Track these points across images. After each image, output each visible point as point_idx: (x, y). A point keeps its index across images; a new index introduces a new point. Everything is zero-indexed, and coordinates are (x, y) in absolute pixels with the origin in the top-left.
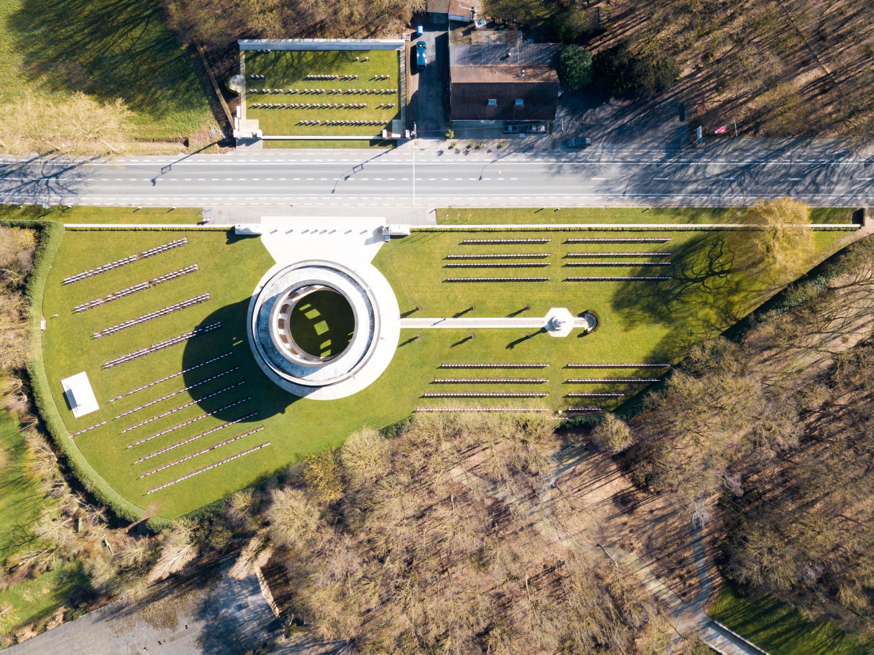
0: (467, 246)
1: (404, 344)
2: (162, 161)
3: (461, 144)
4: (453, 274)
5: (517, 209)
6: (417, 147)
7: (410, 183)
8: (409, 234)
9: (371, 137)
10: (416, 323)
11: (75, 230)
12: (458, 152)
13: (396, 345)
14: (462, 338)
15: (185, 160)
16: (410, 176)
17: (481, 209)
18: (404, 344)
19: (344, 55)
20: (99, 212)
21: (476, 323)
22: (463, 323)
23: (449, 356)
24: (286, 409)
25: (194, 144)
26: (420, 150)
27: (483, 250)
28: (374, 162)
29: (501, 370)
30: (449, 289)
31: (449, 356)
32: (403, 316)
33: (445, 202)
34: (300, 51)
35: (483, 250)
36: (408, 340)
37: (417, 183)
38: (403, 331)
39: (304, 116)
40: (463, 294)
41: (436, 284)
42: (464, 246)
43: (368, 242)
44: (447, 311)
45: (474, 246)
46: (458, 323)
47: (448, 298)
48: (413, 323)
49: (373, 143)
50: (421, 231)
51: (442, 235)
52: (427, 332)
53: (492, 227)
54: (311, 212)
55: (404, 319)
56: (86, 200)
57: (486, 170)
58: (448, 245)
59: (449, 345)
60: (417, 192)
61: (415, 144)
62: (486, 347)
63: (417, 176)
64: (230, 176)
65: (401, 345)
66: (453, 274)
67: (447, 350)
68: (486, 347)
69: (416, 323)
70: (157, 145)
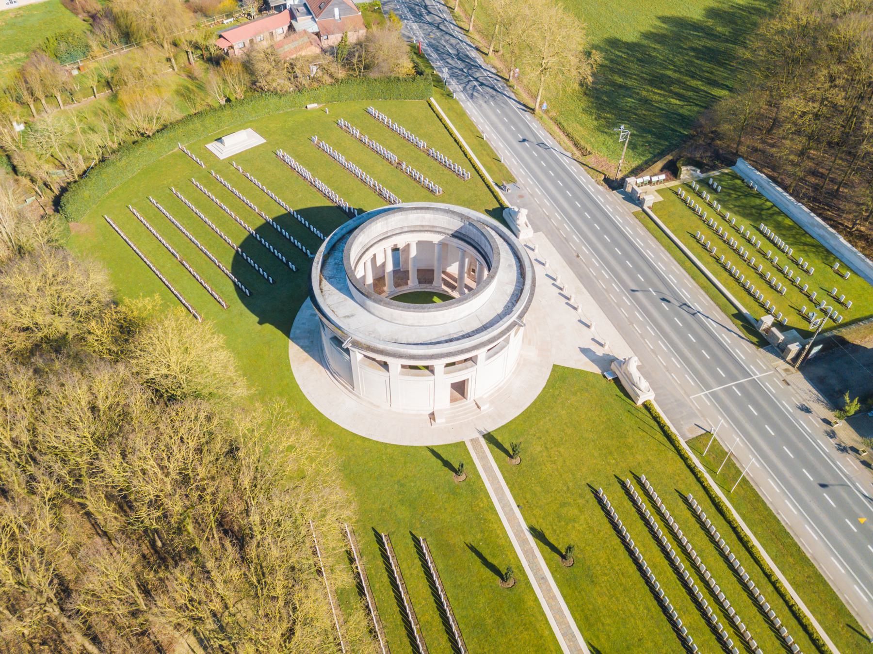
0: (683, 506)
1: (438, 456)
2: (549, 142)
3: (846, 433)
4: (612, 498)
5: (825, 583)
6: (784, 374)
7: (720, 381)
8: (640, 403)
9: (744, 311)
10: (487, 467)
11: (466, 155)
12: (832, 435)
13: (429, 444)
14: (495, 562)
15: (565, 158)
16: (733, 378)
17: (767, 509)
18: (438, 456)
19: (827, 254)
20: (461, 116)
21: (542, 579)
22: (528, 553)
23: (446, 549)
24: (268, 327)
25: (590, 160)
26: (788, 387)
27: (695, 542)
28: (712, 326)
29: (426, 591)
30: (581, 501)
31: (446, 549)
32: (490, 438)
33: (734, 443)
34: (807, 233)
35: (695, 542)
36: (450, 462)
37: (728, 391)
38: (461, 445)
39: (703, 235)
40: (584, 528)
41: (579, 475)
42: (680, 501)
43: (585, 351)
44: (537, 511)
45: (693, 520)
46: (523, 542)
47: (563, 505)
48: (483, 458)
49: (739, 316)
50: (656, 419)
51: (672, 454)
52: (476, 489)
53: (754, 541)
54: (583, 278)
55: (483, 441)
56: (470, 108)
57: (839, 489)
58: (661, 474)
59: (470, 540)
60: (714, 394)
61: (786, 370)
62: (499, 623)
63: (740, 387)
64: (632, 262)
65: (432, 451)
66: (612, 498)
67: (458, 540)
68: (499, 623)
69: (487, 467)
70: (566, 139)
